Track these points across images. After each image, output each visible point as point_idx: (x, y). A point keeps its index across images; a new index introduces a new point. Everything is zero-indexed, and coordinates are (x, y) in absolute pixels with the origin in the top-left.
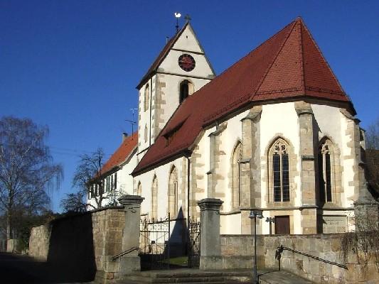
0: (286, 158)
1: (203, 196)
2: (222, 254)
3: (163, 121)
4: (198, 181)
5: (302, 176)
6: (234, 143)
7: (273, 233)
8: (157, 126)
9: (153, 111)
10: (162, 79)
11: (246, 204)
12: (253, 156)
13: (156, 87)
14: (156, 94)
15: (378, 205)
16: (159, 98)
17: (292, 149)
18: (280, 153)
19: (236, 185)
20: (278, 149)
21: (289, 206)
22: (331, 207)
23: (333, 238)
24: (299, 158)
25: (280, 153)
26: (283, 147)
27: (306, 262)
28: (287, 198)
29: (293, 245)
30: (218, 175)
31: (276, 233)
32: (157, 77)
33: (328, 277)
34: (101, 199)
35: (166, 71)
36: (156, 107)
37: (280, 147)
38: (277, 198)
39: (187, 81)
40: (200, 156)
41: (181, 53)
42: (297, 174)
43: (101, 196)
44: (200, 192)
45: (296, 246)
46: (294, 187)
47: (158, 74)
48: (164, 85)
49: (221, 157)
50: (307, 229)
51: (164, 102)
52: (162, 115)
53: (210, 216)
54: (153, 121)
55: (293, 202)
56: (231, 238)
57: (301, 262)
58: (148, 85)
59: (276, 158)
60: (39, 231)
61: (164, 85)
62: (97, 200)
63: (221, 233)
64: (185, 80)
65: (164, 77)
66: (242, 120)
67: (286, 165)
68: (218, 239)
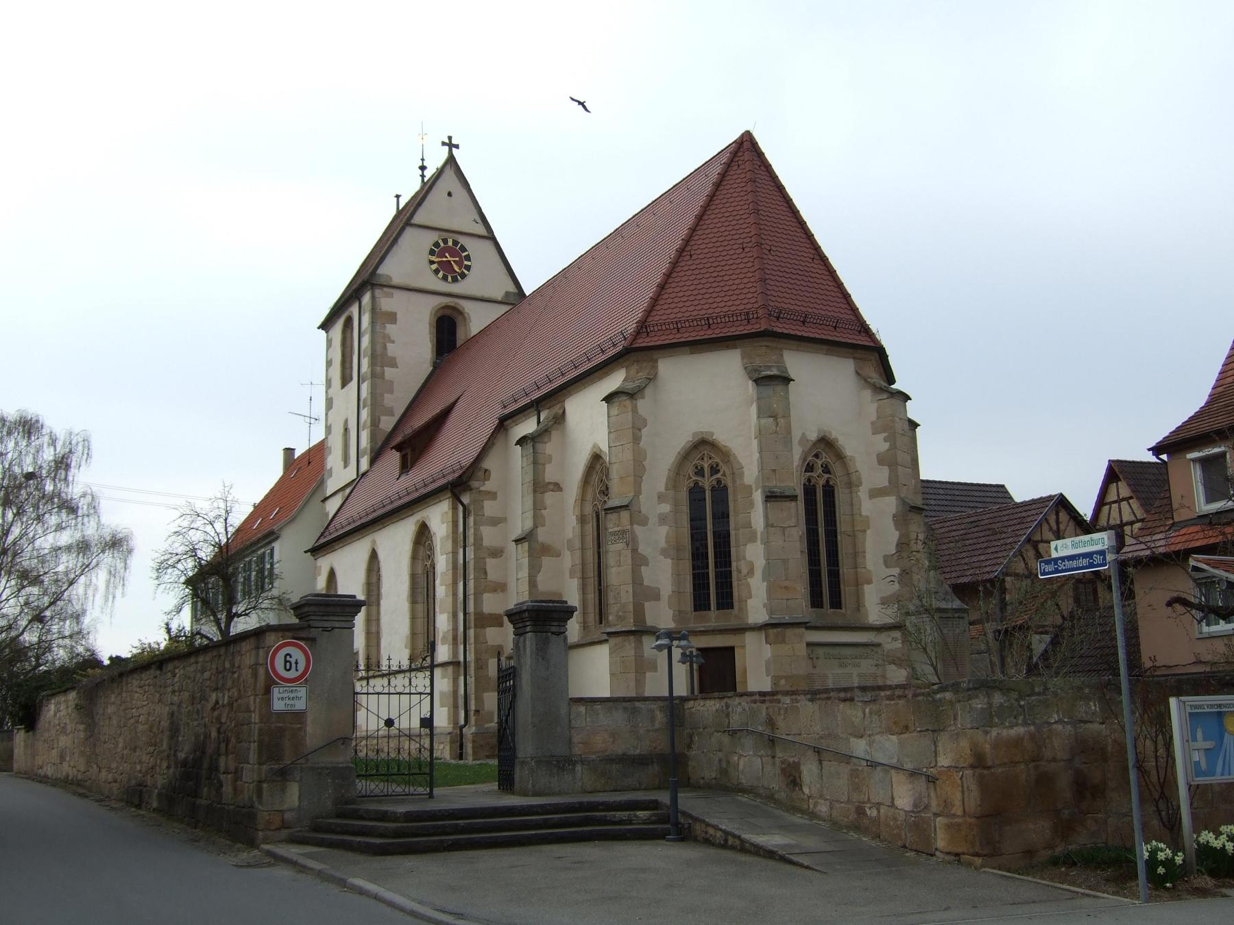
0: (721, 492)
1: (517, 594)
2: (577, 750)
3: (390, 412)
4: (491, 563)
5: (766, 543)
6: (181, 613)
7: (696, 692)
8: (375, 423)
9: (365, 387)
10: (388, 303)
11: (620, 618)
12: (638, 492)
13: (373, 322)
14: (373, 342)
15: (1231, 585)
16: (379, 348)
17: (737, 472)
18: (707, 483)
19: (591, 572)
20: (700, 472)
21: (733, 623)
22: (840, 622)
23: (890, 698)
24: (758, 497)
25: (707, 483)
26: (714, 470)
27: (809, 770)
28: (726, 600)
29: (771, 723)
30: (543, 545)
31: (701, 691)
32: (373, 298)
33: (878, 805)
34: (231, 617)
35: (396, 281)
36: (374, 375)
37: (706, 466)
38: (701, 603)
39: (454, 309)
40: (492, 495)
41: (434, 237)
42: (752, 538)
43: (229, 611)
44: (495, 590)
45: (780, 722)
46: (745, 571)
47: (378, 292)
48: (392, 317)
49: (549, 498)
50: (783, 682)
51: (393, 363)
52: (387, 396)
53: (542, 651)
54: (365, 414)
55: (743, 610)
56: (598, 707)
57: (796, 766)
58: (349, 321)
59: (696, 494)
60: (63, 707)
61: (392, 317)
62: (218, 622)
63: (574, 693)
64: (447, 307)
65: (391, 296)
66: (608, 399)
67: (722, 516)
68: (564, 711)
